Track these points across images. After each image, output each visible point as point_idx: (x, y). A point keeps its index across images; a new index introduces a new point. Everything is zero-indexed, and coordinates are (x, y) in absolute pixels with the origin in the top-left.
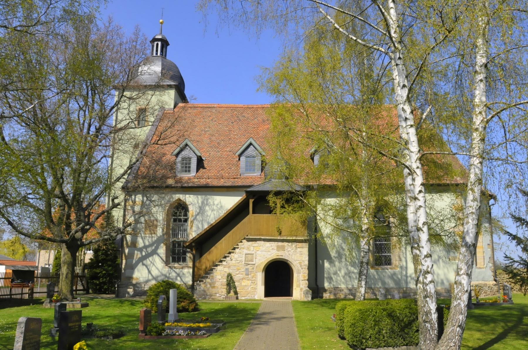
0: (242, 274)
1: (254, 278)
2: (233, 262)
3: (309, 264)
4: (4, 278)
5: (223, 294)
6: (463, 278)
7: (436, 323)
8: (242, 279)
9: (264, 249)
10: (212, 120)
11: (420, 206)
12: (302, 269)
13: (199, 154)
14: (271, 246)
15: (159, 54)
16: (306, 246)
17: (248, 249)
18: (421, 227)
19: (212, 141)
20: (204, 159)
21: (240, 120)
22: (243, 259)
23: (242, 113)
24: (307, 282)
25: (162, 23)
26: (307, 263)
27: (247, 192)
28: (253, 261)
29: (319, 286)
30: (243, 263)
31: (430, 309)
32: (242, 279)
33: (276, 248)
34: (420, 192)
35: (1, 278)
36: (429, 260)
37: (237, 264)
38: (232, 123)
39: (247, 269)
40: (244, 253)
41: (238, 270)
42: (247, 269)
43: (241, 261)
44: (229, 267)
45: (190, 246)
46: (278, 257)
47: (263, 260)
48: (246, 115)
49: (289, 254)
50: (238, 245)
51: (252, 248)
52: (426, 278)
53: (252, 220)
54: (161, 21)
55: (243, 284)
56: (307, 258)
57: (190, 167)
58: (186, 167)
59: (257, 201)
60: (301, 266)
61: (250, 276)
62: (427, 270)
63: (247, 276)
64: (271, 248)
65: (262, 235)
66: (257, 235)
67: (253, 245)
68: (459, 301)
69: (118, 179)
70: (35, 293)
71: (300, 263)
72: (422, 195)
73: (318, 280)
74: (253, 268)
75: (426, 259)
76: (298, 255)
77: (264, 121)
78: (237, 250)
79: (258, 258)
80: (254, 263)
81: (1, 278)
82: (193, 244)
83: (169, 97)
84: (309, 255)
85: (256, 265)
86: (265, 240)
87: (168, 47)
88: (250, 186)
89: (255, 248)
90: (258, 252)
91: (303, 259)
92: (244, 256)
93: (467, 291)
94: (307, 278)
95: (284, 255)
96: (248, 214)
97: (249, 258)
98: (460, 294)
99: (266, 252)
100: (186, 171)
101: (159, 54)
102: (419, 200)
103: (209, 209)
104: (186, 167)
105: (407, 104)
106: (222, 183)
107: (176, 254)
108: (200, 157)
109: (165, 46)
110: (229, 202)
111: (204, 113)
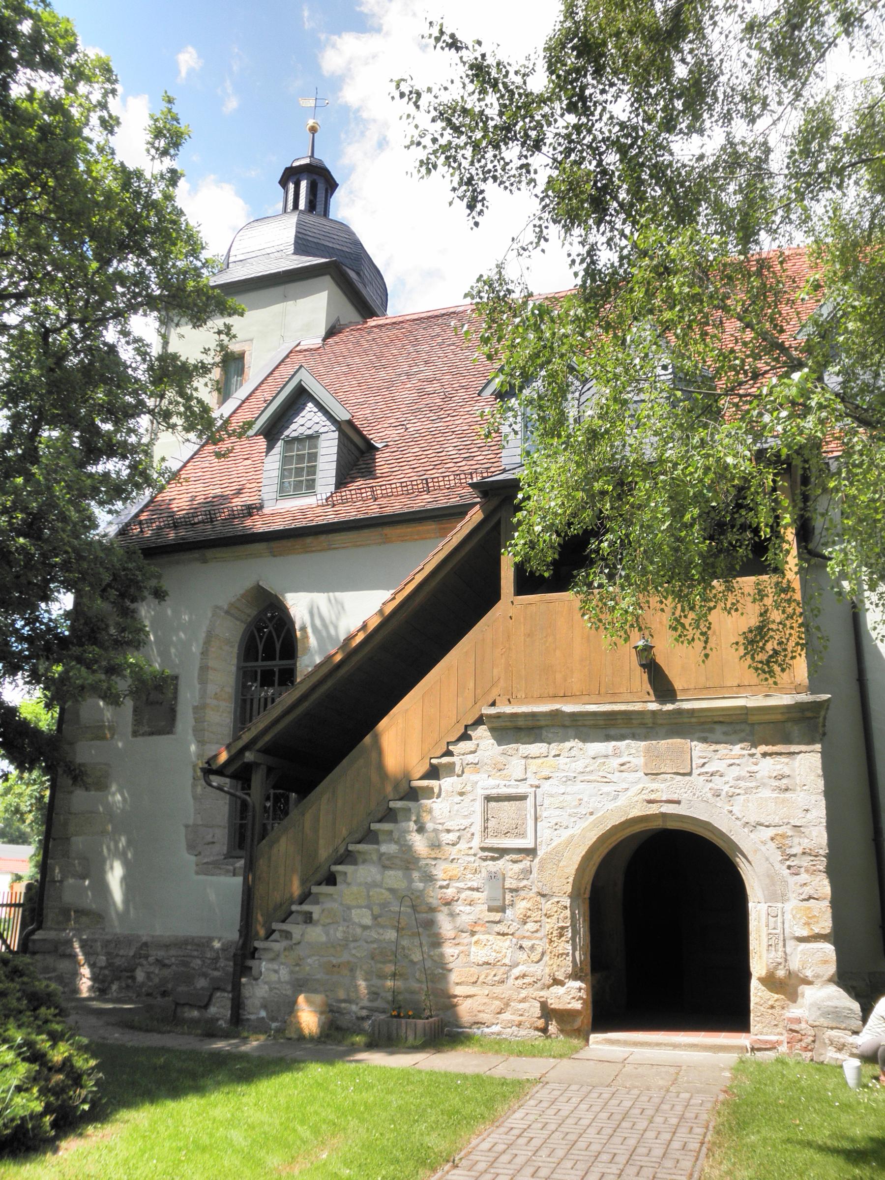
3: (828, 815)
4: (7, 905)
13: (343, 415)
15: (302, 205)
16: (806, 765)
24: (828, 949)
25: (313, 130)
26: (818, 837)
28: (523, 835)
35: (2, 905)
40: (480, 793)
46: (654, 809)
50: (449, 753)
54: (311, 122)
56: (819, 812)
58: (299, 472)
63: (497, 916)
64: (615, 763)
66: (541, 698)
78: (447, 783)
79: (549, 814)
80: (527, 843)
81: (2, 905)
83: (313, 309)
84: (829, 793)
89: (533, 765)
92: (478, 806)
94: (825, 925)
95: (684, 797)
96: (492, 597)
99: (594, 792)
100: (298, 486)
101: (302, 205)
104: (299, 472)
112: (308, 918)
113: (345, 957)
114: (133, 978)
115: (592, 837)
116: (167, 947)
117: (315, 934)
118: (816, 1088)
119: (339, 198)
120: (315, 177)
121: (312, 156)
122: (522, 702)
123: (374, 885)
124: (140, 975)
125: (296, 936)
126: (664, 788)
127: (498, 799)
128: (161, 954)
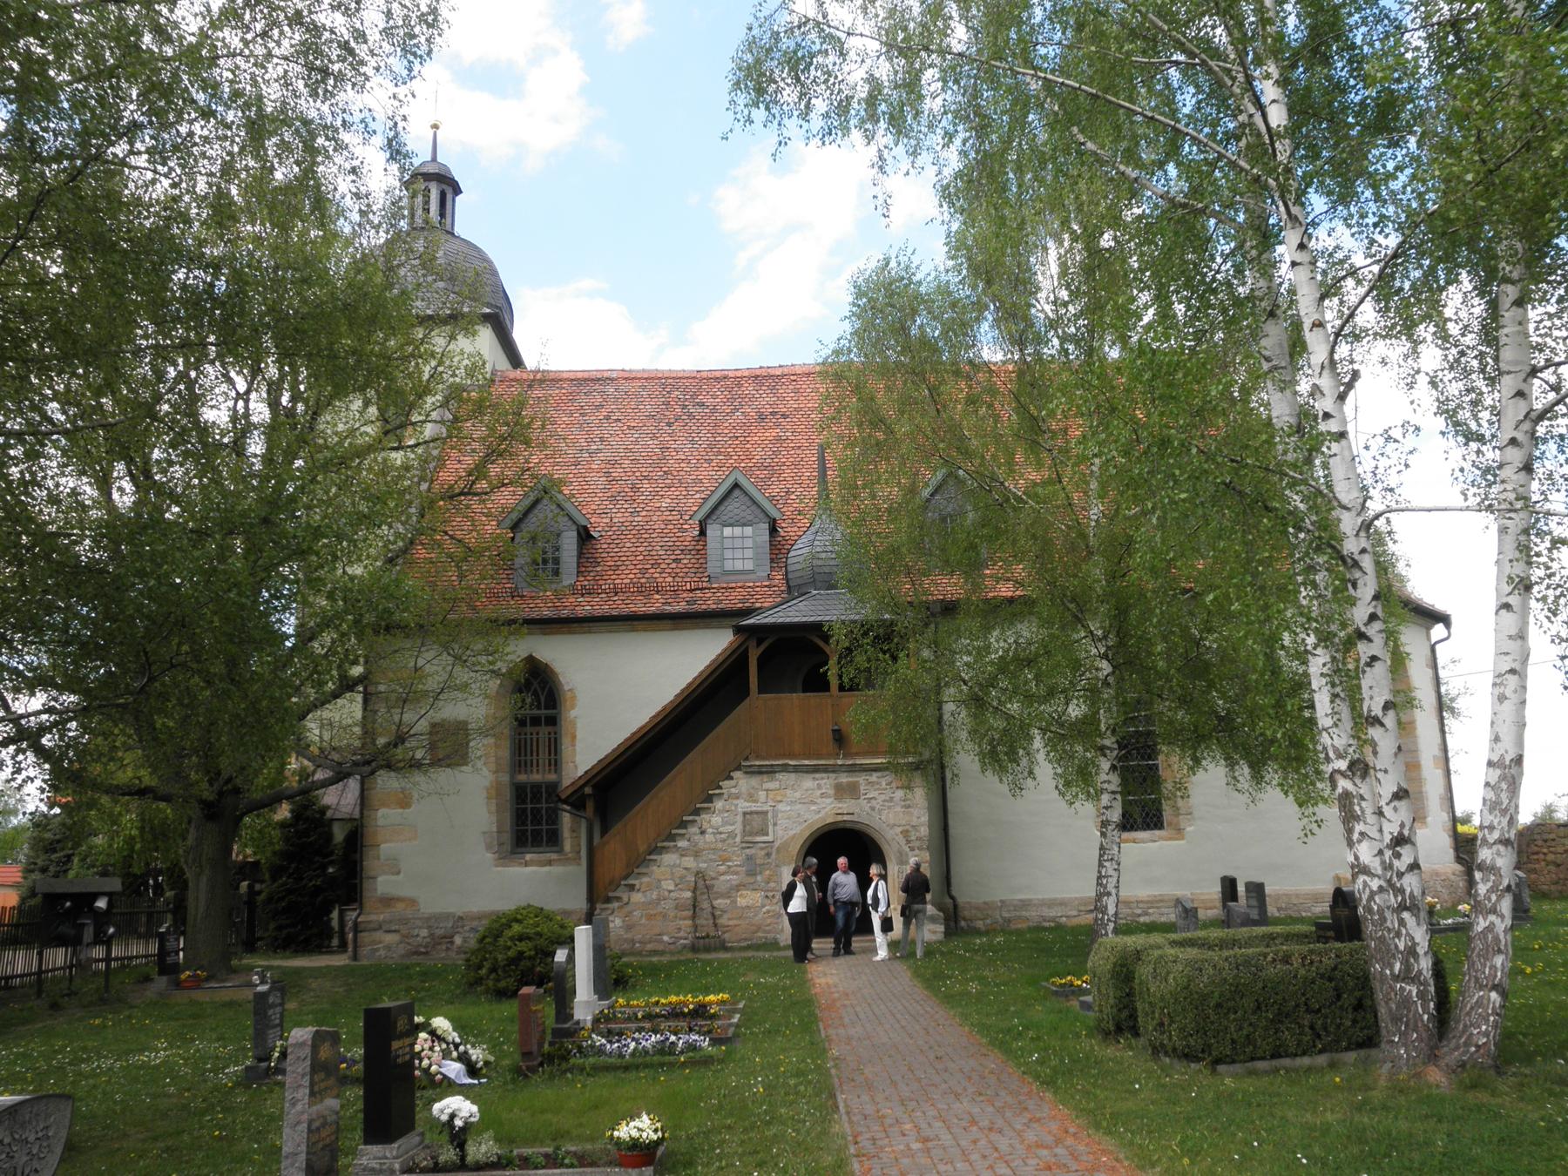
0: (736, 873)
1: (772, 885)
2: (709, 837)
5: (682, 934)
6: (1498, 854)
7: (1432, 982)
8: (739, 887)
9: (798, 795)
10: (608, 418)
11: (1374, 658)
12: (912, 849)
14: (819, 786)
17: (751, 798)
18: (1380, 714)
19: (612, 480)
20: (595, 535)
21: (691, 416)
22: (738, 828)
23: (695, 396)
26: (924, 831)
27: (738, 630)
29: (961, 900)
30: (738, 839)
31: (1415, 944)
32: (739, 887)
33: (832, 792)
34: (1373, 617)
36: (1402, 805)
37: (720, 845)
38: (669, 424)
39: (749, 858)
41: (725, 860)
42: (749, 858)
43: (732, 835)
44: (697, 854)
45: (577, 801)
46: (840, 818)
47: (797, 830)
48: (709, 401)
49: (873, 809)
51: (762, 794)
52: (1398, 856)
53: (762, 709)
55: (741, 902)
57: (557, 561)
59: (777, 659)
60: (908, 842)
61: (759, 878)
62: (1401, 833)
65: (792, 756)
66: (777, 757)
67: (766, 786)
68: (1492, 918)
69: (1513, 675)
70: (40, 954)
71: (905, 833)
72: (1377, 625)
73: (954, 881)
74: (768, 855)
75: (1396, 803)
76: (898, 809)
77: (762, 417)
80: (769, 838)
82: (588, 790)
85: (777, 844)
86: (797, 769)
87: (458, 199)
88: (748, 612)
89: (771, 795)
90: (781, 807)
91: (915, 821)
92: (739, 818)
93: (1509, 888)
96: (744, 693)
97: (755, 823)
98: (1494, 898)
99: (799, 804)
102: (1370, 640)
103: (619, 689)
105: (1326, 373)
106: (656, 604)
107: (530, 821)
108: (585, 528)
109: (449, 197)
110: (687, 659)
111: (583, 400)
112: (632, 887)
113: (660, 909)
114: (452, 943)
115: (807, 834)
116: (480, 918)
117: (637, 897)
118: (1460, 439)
119: (463, 205)
120: (444, 186)
121: (434, 159)
122: (764, 759)
123: (674, 866)
124: (458, 940)
125: (625, 899)
126: (847, 806)
127: (751, 813)
128: (475, 923)
